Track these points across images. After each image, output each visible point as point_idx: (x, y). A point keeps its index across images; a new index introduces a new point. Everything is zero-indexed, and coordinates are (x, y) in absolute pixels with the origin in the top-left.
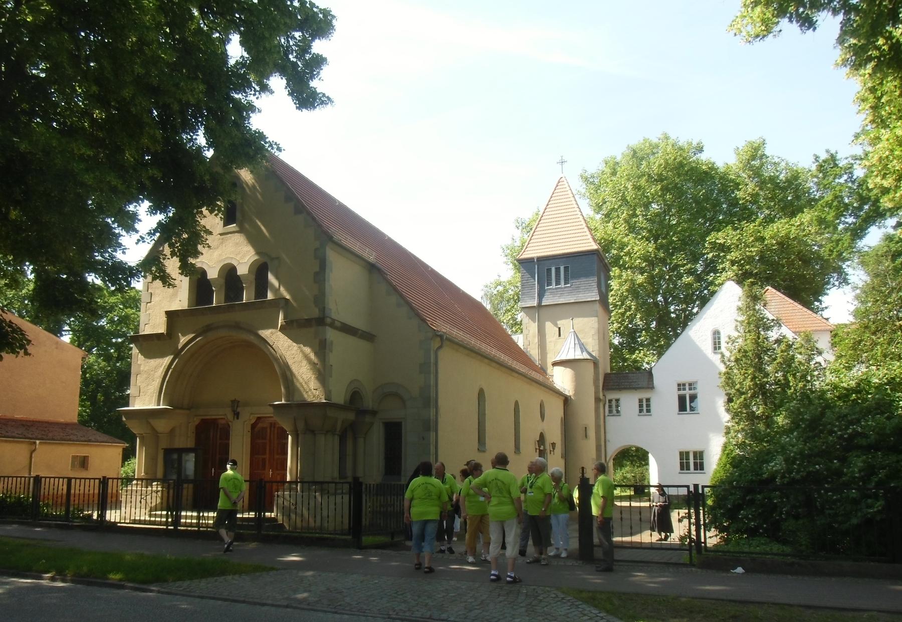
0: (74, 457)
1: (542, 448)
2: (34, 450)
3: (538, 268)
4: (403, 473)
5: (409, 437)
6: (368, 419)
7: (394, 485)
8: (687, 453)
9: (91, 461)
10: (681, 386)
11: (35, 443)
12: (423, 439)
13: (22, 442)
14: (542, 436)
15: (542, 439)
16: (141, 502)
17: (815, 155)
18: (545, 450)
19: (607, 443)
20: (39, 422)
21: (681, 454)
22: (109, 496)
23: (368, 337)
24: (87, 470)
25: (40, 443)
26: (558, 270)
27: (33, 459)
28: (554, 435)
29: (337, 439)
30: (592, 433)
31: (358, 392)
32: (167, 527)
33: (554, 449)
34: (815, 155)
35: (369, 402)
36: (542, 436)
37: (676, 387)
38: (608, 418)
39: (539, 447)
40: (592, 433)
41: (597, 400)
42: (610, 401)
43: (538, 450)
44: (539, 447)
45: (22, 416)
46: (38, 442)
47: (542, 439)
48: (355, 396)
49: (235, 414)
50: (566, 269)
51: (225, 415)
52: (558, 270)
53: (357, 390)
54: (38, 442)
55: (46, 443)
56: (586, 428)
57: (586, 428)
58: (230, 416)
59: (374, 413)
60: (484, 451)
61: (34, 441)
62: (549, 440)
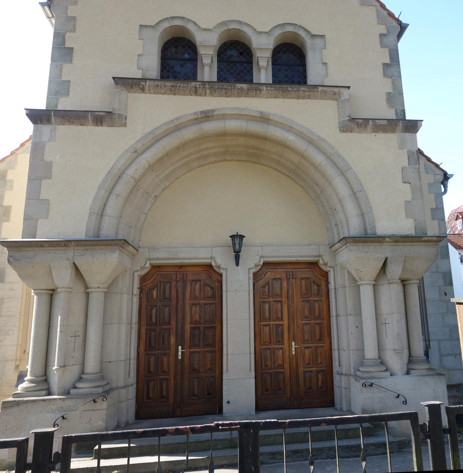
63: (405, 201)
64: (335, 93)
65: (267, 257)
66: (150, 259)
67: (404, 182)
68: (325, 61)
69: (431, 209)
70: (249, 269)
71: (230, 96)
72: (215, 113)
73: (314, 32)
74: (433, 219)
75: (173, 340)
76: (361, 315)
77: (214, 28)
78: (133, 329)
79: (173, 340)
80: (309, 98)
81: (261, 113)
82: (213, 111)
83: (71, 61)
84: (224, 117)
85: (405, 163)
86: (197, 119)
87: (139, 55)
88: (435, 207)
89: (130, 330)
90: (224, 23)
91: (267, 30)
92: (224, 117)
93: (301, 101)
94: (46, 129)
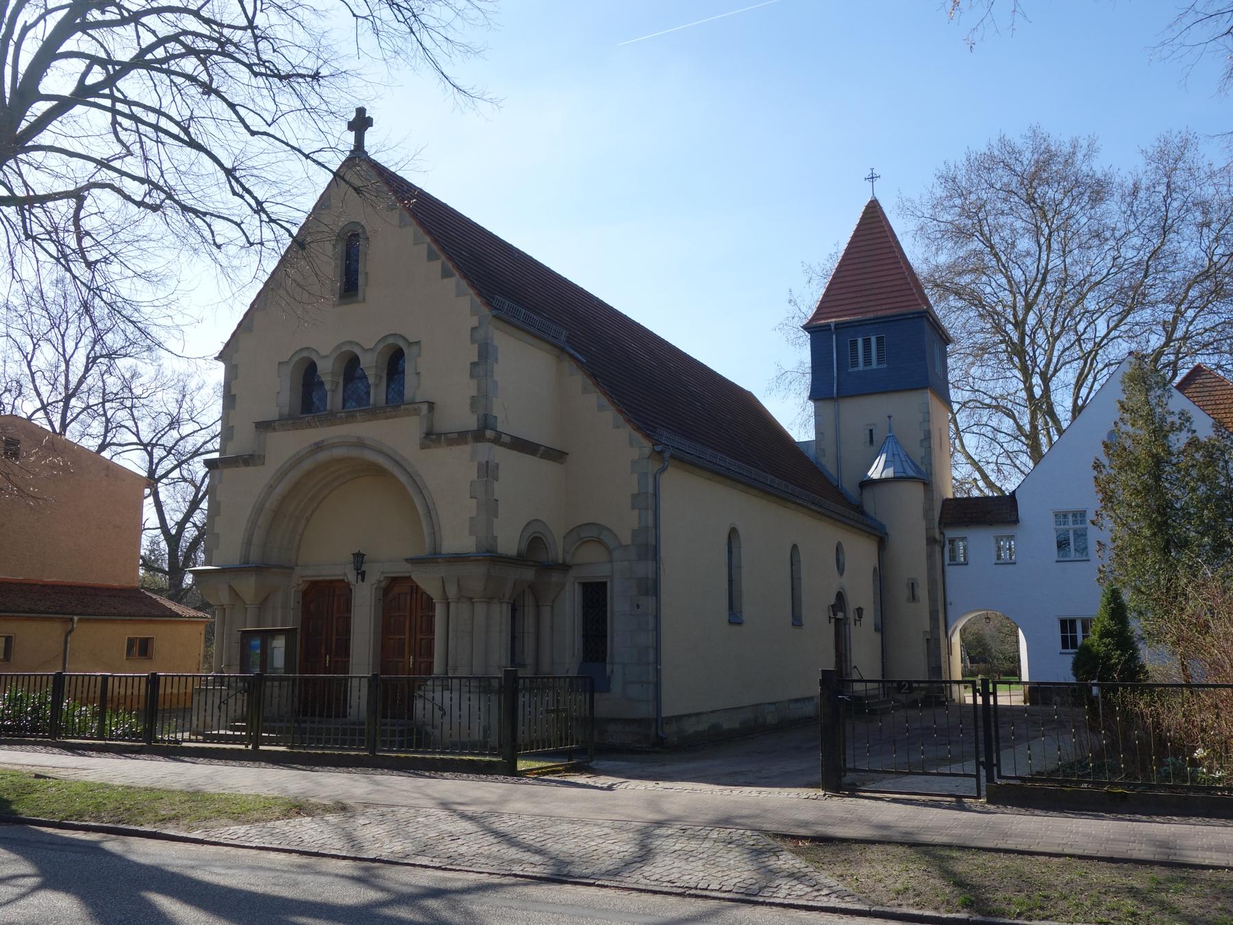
0: (131, 642)
1: (840, 615)
2: (71, 631)
3: (837, 340)
4: (608, 659)
5: (618, 604)
6: (555, 578)
7: (105, 678)
8: (1073, 622)
9: (157, 645)
10: (1061, 516)
11: (72, 620)
12: (638, 606)
13: (52, 619)
14: (840, 596)
15: (840, 600)
16: (220, 708)
17: (361, 111)
18: (846, 618)
19: (949, 607)
20: (80, 587)
21: (1063, 623)
22: (161, 699)
23: (556, 455)
24: (150, 658)
25: (79, 620)
26: (867, 343)
27: (68, 645)
28: (862, 594)
29: (506, 610)
30: (923, 592)
31: (541, 539)
32: (256, 747)
33: (860, 617)
34: (361, 111)
35: (558, 550)
36: (840, 596)
37: (1052, 519)
38: (948, 569)
39: (835, 614)
40: (923, 592)
41: (931, 541)
42: (952, 541)
43: (833, 620)
44: (835, 614)
45: (55, 579)
46: (76, 618)
47: (840, 600)
48: (536, 542)
49: (358, 574)
50: (880, 341)
51: (345, 574)
52: (867, 343)
53: (540, 536)
54: (76, 618)
55: (88, 620)
56: (913, 584)
57: (913, 584)
58: (351, 577)
59: (565, 567)
60: (740, 624)
61: (70, 616)
62: (852, 604)
63: (471, 518)
64: (415, 410)
65: (387, 573)
66: (303, 577)
67: (471, 497)
68: (418, 371)
69: (632, 495)
70: (372, 585)
71: (335, 425)
72: (325, 443)
73: (411, 340)
74: (633, 508)
75: (323, 651)
76: (512, 637)
77: (331, 353)
78: (1006, 835)
79: (323, 651)
80: (396, 417)
81: (358, 438)
82: (323, 441)
83: (234, 409)
84: (333, 446)
85: (474, 475)
86: (312, 451)
87: (278, 393)
88: (637, 492)
89: (1011, 844)
90: (338, 347)
91: (372, 346)
92: (333, 446)
93: (390, 420)
94: (217, 472)
